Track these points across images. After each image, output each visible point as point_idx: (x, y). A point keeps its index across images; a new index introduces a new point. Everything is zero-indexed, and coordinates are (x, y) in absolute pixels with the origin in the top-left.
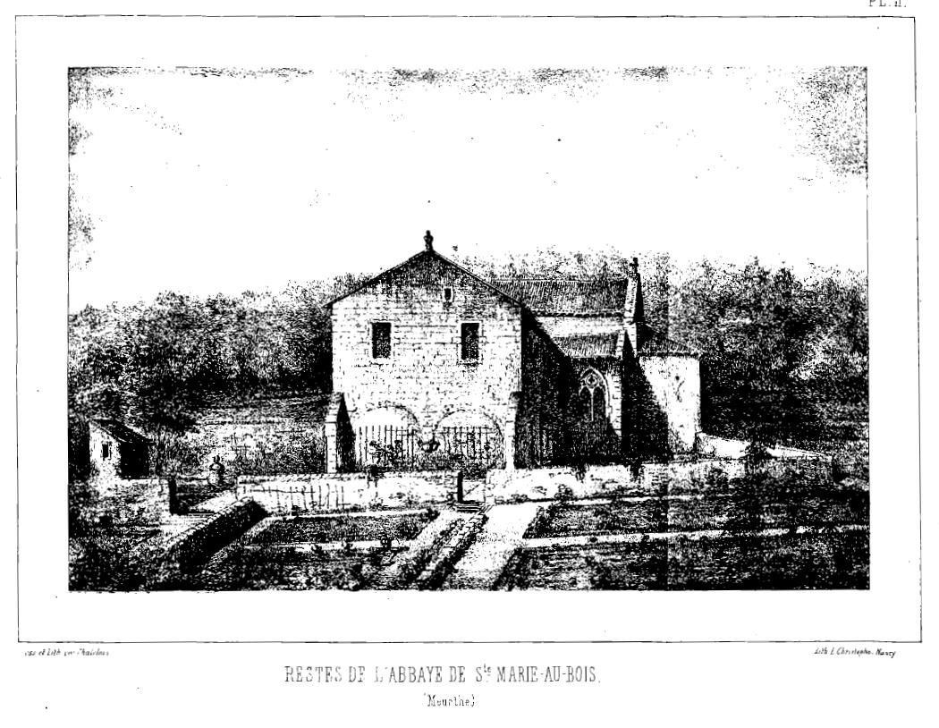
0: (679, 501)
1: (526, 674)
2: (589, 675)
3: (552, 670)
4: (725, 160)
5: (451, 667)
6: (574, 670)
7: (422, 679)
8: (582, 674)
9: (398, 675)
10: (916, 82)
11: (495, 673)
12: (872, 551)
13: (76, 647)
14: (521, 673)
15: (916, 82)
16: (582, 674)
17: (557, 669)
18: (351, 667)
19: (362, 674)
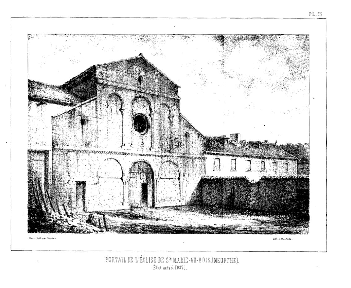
0: (152, 229)
1: (224, 260)
2: (151, 260)
3: (193, 259)
4: (187, 190)
5: (159, 258)
6: (108, 258)
7: (120, 261)
8: (234, 260)
9: (143, 260)
10: (11, 85)
11: (173, 259)
12: (27, 226)
13: (182, 35)
14: (225, 260)
15: (11, 85)
16: (234, 260)
17: (195, 259)
18: (128, 258)
19: (163, 260)
